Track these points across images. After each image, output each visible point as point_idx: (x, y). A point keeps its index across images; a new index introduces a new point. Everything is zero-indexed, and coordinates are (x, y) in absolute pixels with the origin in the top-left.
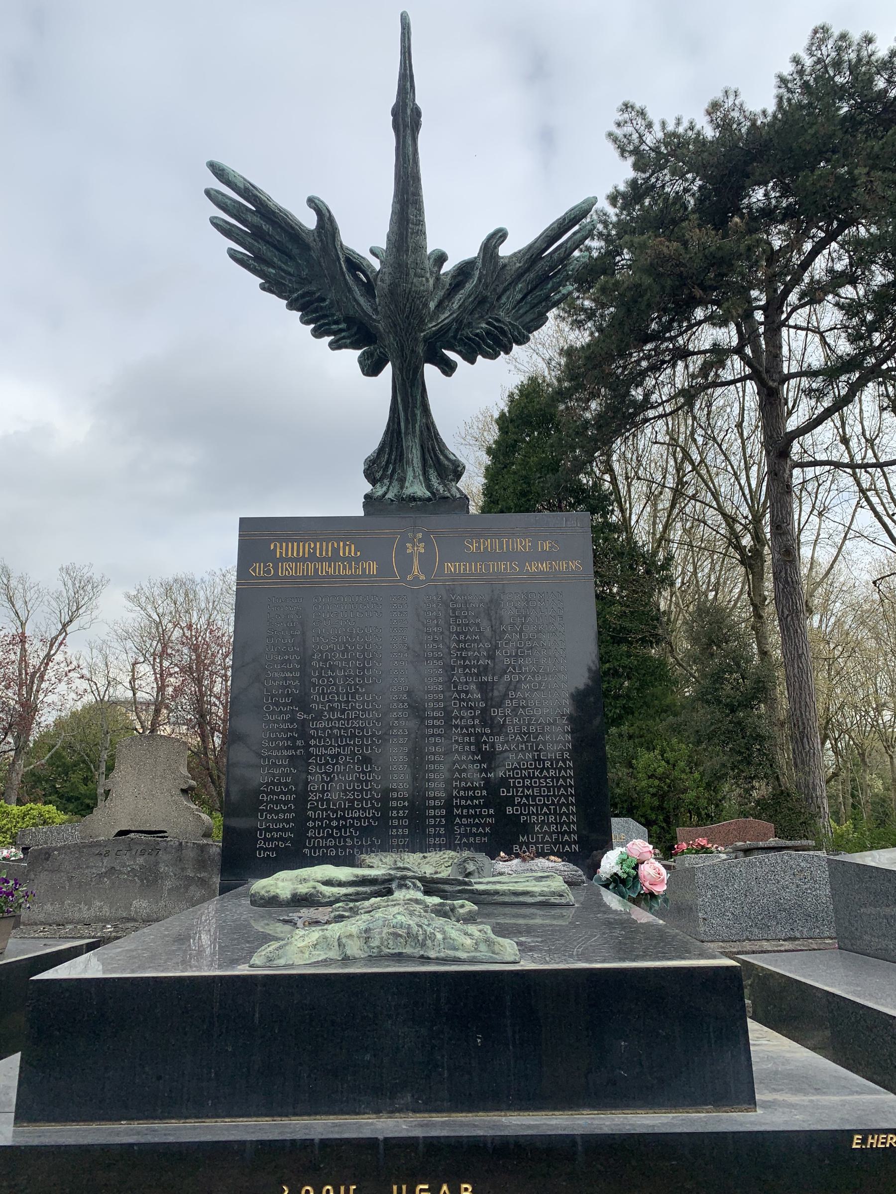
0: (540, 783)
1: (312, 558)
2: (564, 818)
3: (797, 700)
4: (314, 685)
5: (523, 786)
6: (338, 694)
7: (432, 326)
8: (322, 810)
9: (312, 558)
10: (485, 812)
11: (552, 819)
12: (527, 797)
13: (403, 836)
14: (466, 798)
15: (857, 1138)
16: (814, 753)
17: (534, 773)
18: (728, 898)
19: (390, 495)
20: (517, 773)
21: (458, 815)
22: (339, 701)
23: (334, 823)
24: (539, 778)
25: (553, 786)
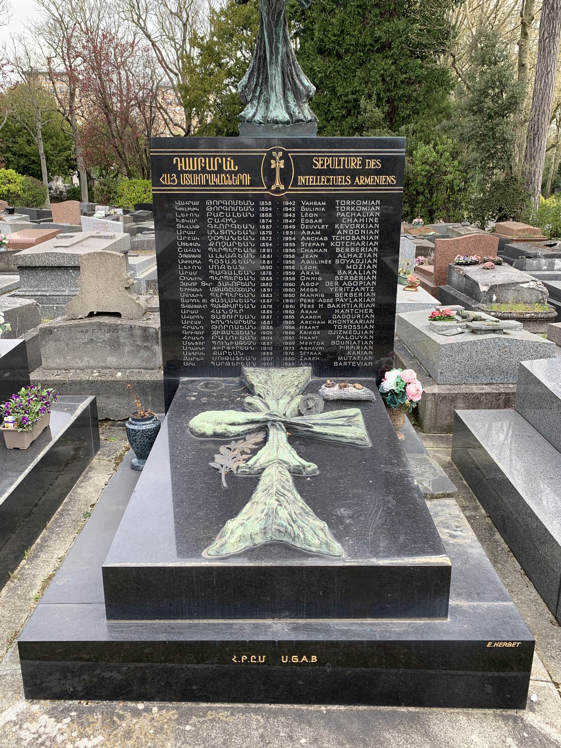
0: (353, 327)
1: (204, 170)
3: (538, 108)
4: (211, 264)
5: (342, 329)
6: (227, 270)
8: (221, 341)
9: (204, 170)
12: (344, 335)
13: (270, 356)
14: (307, 336)
15: (490, 644)
16: (541, 149)
17: (349, 322)
18: (457, 362)
20: (339, 322)
21: (302, 345)
22: (227, 275)
24: (353, 325)
25: (361, 329)
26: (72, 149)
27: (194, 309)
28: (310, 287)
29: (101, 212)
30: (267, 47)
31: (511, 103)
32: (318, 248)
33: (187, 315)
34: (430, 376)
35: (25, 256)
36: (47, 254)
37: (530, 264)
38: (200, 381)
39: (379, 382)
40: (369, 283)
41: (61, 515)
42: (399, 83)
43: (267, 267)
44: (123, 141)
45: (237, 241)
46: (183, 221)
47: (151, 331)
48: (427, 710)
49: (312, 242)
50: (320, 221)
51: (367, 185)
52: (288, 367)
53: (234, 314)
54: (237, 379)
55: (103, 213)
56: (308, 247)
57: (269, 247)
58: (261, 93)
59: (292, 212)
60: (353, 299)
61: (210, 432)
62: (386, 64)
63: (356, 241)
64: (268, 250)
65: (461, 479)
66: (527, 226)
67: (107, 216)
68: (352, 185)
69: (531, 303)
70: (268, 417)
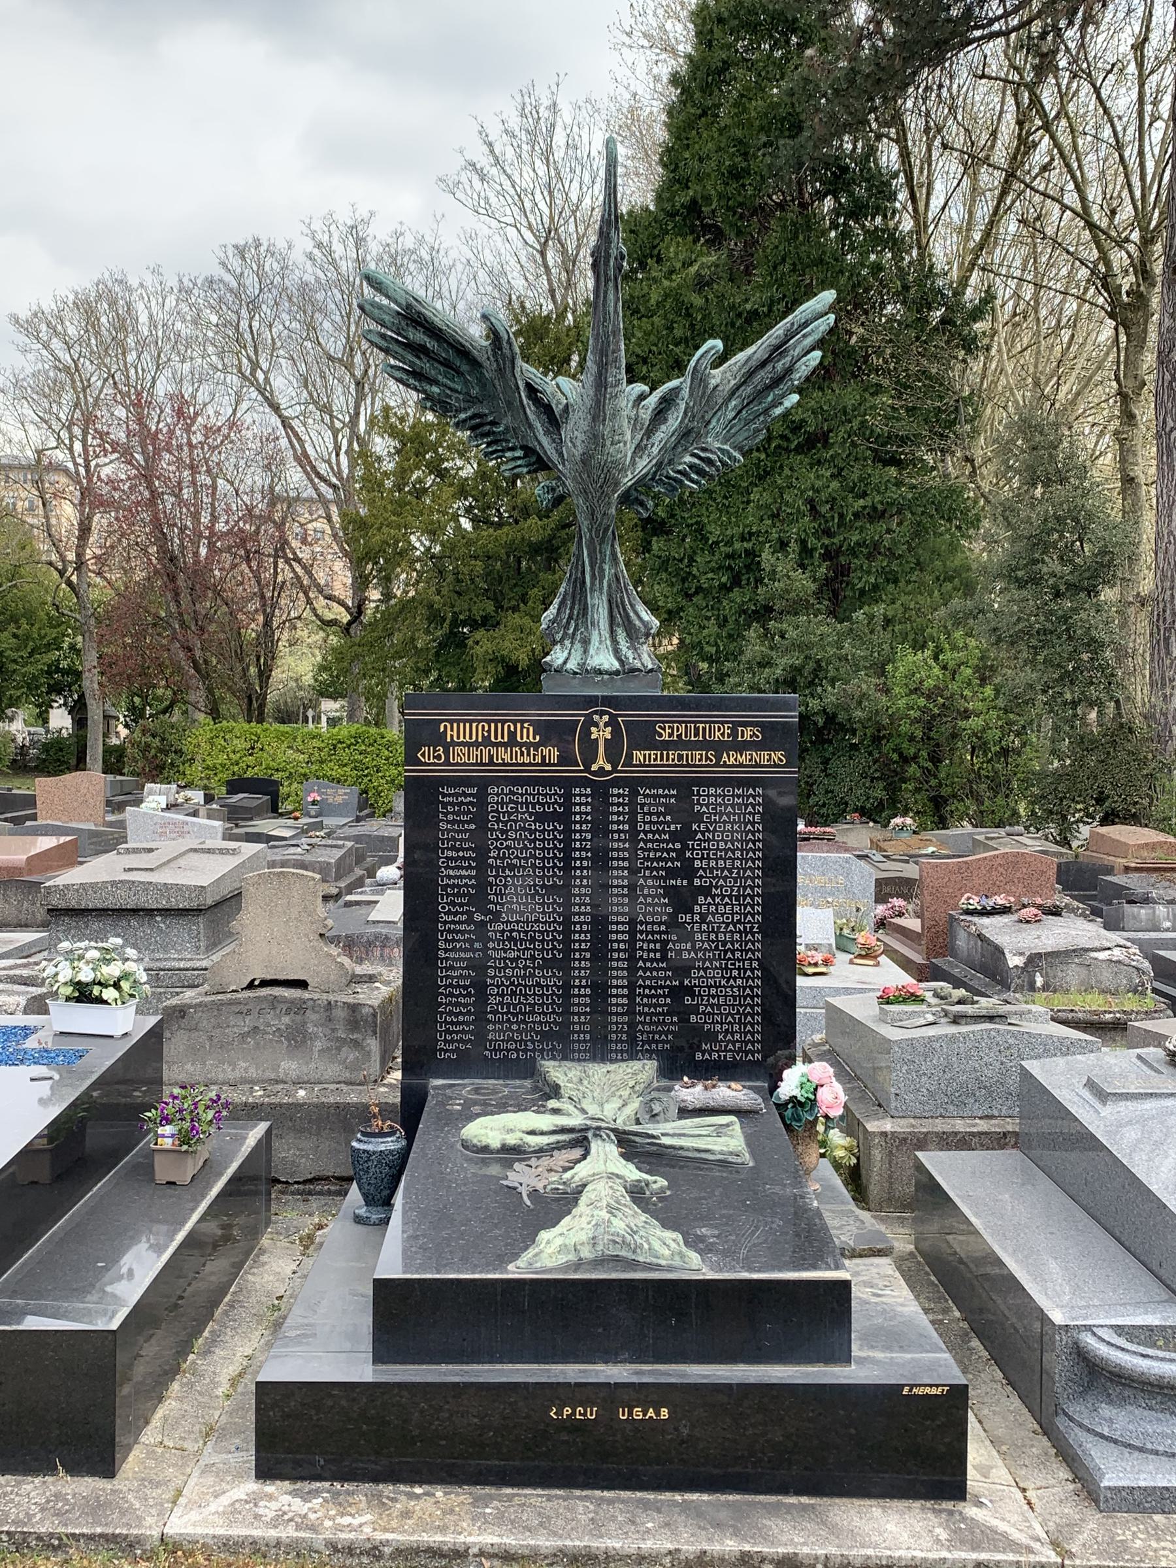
1: (487, 742)
2: (749, 1028)
4: (491, 885)
6: (517, 894)
7: (627, 480)
10: (668, 1019)
11: (736, 1028)
12: (712, 1006)
13: (585, 1041)
14: (649, 1006)
15: (906, 1389)
19: (570, 666)
23: (515, 1027)
26: (65, 646)
27: (460, 959)
28: (653, 923)
29: (157, 798)
30: (588, 568)
31: (1102, 565)
32: (666, 860)
33: (447, 969)
34: (880, 1105)
35: (67, 887)
36: (114, 883)
37: (1134, 918)
38: (466, 1086)
39: (774, 1087)
40: (749, 918)
41: (231, 1306)
42: (850, 517)
43: (583, 891)
44: (206, 636)
45: (535, 848)
46: (450, 817)
47: (365, 1010)
48: (826, 1501)
49: (656, 851)
50: (668, 818)
51: (741, 765)
52: (616, 1060)
53: (525, 967)
54: (528, 1083)
55: (163, 801)
56: (648, 859)
57: (587, 858)
58: (576, 629)
59: (623, 805)
60: (724, 943)
61: (495, 1144)
62: (818, 477)
63: (726, 850)
64: (585, 864)
65: (927, 1274)
66: (1162, 837)
67: (170, 807)
68: (717, 765)
69: (1115, 993)
70: (589, 1122)
